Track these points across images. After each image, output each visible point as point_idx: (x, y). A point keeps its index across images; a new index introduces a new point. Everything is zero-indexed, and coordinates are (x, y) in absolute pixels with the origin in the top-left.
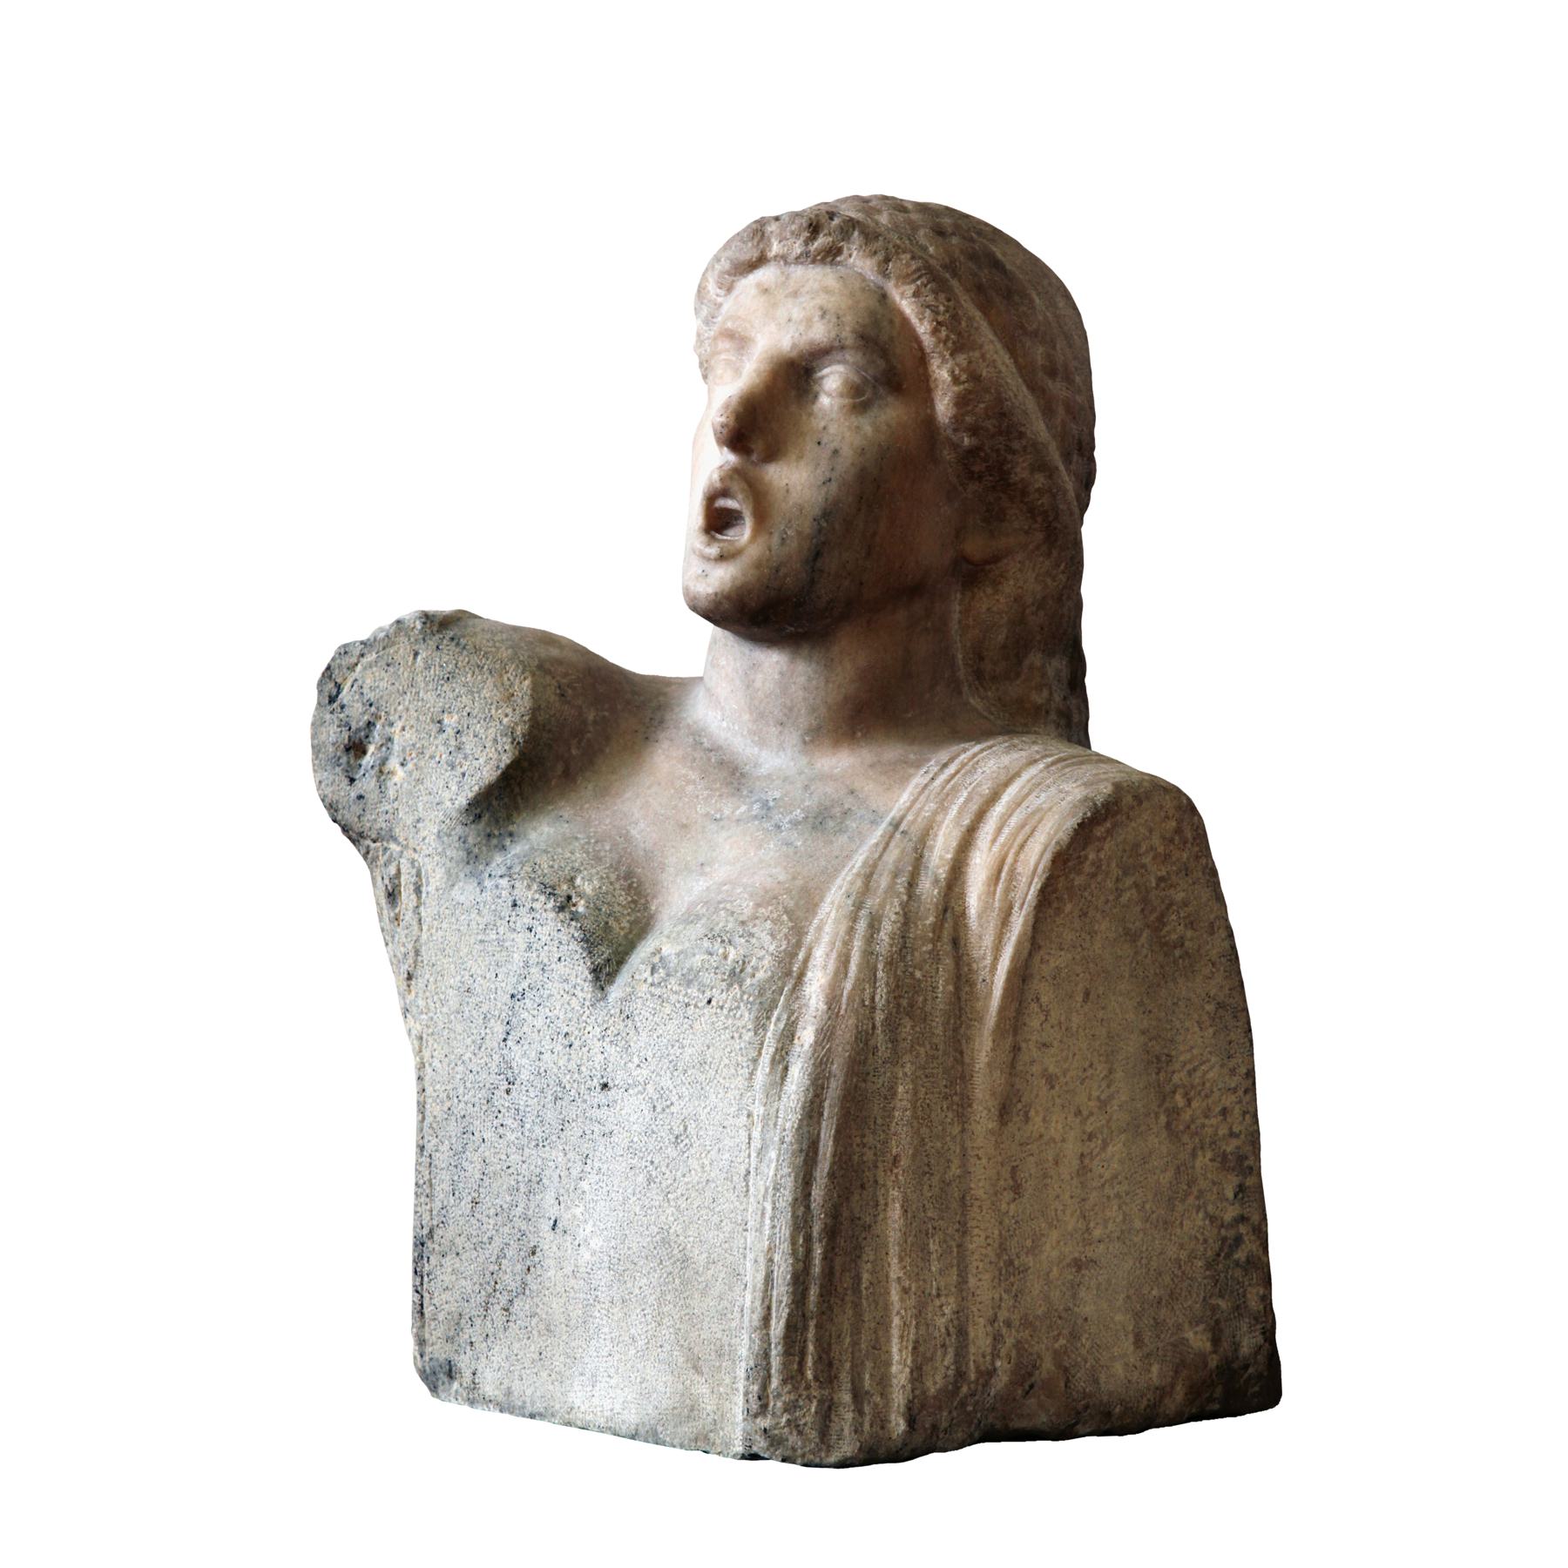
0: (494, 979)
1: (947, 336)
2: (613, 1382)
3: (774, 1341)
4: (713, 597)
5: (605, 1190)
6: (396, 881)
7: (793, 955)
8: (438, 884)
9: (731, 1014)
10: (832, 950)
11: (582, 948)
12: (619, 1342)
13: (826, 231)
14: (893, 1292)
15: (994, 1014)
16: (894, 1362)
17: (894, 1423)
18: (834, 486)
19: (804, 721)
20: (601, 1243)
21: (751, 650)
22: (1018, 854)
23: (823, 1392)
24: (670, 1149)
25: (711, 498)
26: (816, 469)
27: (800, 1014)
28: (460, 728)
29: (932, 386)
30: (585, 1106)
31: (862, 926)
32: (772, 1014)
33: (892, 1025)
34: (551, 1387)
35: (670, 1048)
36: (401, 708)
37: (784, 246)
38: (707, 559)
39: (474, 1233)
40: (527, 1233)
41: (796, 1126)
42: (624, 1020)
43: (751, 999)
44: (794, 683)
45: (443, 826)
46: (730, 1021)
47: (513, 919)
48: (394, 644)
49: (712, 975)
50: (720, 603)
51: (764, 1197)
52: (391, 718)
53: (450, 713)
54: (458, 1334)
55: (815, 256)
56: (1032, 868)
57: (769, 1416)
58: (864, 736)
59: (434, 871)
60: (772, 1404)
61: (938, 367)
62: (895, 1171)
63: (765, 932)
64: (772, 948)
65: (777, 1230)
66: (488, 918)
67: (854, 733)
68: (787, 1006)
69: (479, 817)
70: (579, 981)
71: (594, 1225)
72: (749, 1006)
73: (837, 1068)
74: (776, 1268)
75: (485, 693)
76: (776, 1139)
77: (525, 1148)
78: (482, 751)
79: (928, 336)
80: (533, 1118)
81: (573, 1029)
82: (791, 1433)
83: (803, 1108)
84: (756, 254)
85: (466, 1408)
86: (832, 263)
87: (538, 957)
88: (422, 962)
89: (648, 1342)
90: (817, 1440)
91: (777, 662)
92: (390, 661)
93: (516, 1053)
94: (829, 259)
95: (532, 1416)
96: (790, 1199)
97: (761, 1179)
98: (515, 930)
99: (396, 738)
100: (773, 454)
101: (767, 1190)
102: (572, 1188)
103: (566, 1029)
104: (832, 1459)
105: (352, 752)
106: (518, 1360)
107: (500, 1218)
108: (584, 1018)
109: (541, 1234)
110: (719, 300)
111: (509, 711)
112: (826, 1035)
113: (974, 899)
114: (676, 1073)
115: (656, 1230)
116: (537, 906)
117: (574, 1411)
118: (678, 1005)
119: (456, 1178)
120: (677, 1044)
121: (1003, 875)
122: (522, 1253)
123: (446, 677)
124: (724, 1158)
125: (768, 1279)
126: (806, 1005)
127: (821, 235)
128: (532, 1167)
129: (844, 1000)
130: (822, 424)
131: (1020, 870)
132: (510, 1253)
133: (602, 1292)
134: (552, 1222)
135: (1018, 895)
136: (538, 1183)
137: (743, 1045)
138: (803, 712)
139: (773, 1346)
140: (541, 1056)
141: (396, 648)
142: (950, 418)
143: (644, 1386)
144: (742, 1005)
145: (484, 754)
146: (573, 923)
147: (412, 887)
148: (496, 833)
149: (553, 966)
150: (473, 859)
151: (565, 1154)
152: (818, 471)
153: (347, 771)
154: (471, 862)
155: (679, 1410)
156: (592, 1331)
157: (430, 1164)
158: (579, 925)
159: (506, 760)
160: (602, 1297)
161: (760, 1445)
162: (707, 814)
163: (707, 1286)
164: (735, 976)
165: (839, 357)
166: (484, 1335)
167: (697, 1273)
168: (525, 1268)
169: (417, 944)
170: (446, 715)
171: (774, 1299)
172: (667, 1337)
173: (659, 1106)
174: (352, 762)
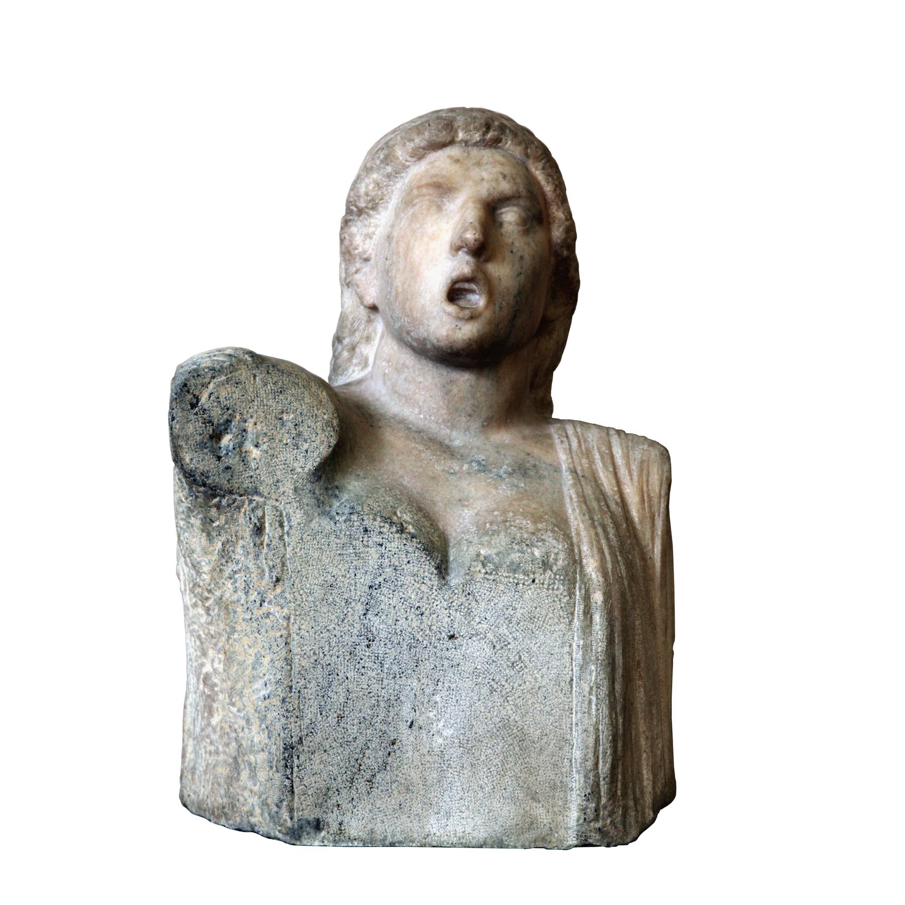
0: (353, 577)
1: (560, 193)
2: (464, 815)
3: (602, 776)
4: (468, 341)
6: (263, 520)
7: (573, 551)
8: (299, 520)
9: (550, 587)
10: (592, 546)
11: (425, 554)
12: (469, 790)
13: (493, 128)
14: (642, 739)
15: (659, 576)
16: (645, 779)
17: (647, 814)
18: (522, 277)
19: (485, 413)
20: (452, 732)
21: (448, 372)
22: (647, 486)
25: (455, 282)
26: (513, 267)
27: (589, 584)
29: (551, 221)
30: (435, 650)
31: (600, 530)
32: (576, 586)
34: (410, 825)
35: (505, 610)
36: (251, 411)
37: (468, 135)
38: (459, 319)
40: (388, 731)
41: (605, 649)
42: (466, 596)
43: (562, 578)
44: (479, 391)
45: (298, 484)
46: (551, 591)
47: (366, 539)
48: (237, 370)
49: (531, 565)
50: (472, 345)
51: (590, 694)
52: (245, 417)
53: (287, 413)
54: (326, 801)
55: (488, 142)
56: (658, 493)
57: (601, 821)
58: (510, 422)
59: (294, 513)
60: (602, 813)
61: (556, 210)
62: (639, 670)
63: (551, 538)
64: (560, 547)
65: (600, 711)
66: (344, 540)
67: (507, 420)
68: (582, 581)
69: (320, 477)
70: (426, 574)
71: (446, 722)
72: (561, 582)
73: (616, 613)
74: (601, 733)
75: (307, 400)
77: (384, 680)
78: (316, 436)
79: (551, 193)
80: (392, 661)
81: (424, 604)
82: (612, 828)
83: (607, 638)
84: (449, 139)
85: (523, 850)
86: (496, 148)
88: (287, 570)
89: (494, 788)
91: (468, 380)
92: (237, 381)
93: (375, 622)
94: (494, 145)
95: (392, 845)
96: (607, 692)
97: (585, 683)
98: (368, 546)
99: (250, 430)
101: (591, 688)
102: (426, 700)
103: (418, 605)
104: (629, 840)
105: (214, 439)
106: (380, 811)
107: (363, 725)
108: (433, 597)
109: (400, 732)
110: (407, 163)
111: (325, 411)
112: (607, 596)
113: (635, 514)
114: (511, 625)
115: (498, 720)
116: (385, 530)
117: (430, 837)
118: (509, 585)
119: (323, 703)
120: (511, 608)
121: (646, 498)
122: (383, 745)
123: (279, 390)
124: (552, 672)
125: (597, 740)
126: (590, 579)
127: (491, 130)
128: (391, 691)
129: (610, 574)
130: (510, 241)
131: (652, 495)
132: (372, 745)
133: (454, 762)
134: (409, 723)
136: (396, 700)
138: (484, 408)
139: (601, 779)
140: (396, 623)
141: (240, 372)
142: (562, 240)
143: (491, 814)
144: (556, 581)
145: (318, 438)
146: (414, 540)
147: (277, 524)
148: (330, 487)
149: (404, 566)
150: (321, 505)
151: (420, 681)
153: (213, 452)
154: (321, 505)
155: (521, 825)
156: (445, 786)
157: (299, 697)
158: (418, 541)
159: (333, 442)
161: (595, 837)
163: (541, 749)
164: (546, 565)
165: (516, 202)
167: (533, 742)
169: (284, 559)
170: (285, 414)
171: (601, 752)
172: (510, 783)
173: (499, 644)
174: (214, 446)
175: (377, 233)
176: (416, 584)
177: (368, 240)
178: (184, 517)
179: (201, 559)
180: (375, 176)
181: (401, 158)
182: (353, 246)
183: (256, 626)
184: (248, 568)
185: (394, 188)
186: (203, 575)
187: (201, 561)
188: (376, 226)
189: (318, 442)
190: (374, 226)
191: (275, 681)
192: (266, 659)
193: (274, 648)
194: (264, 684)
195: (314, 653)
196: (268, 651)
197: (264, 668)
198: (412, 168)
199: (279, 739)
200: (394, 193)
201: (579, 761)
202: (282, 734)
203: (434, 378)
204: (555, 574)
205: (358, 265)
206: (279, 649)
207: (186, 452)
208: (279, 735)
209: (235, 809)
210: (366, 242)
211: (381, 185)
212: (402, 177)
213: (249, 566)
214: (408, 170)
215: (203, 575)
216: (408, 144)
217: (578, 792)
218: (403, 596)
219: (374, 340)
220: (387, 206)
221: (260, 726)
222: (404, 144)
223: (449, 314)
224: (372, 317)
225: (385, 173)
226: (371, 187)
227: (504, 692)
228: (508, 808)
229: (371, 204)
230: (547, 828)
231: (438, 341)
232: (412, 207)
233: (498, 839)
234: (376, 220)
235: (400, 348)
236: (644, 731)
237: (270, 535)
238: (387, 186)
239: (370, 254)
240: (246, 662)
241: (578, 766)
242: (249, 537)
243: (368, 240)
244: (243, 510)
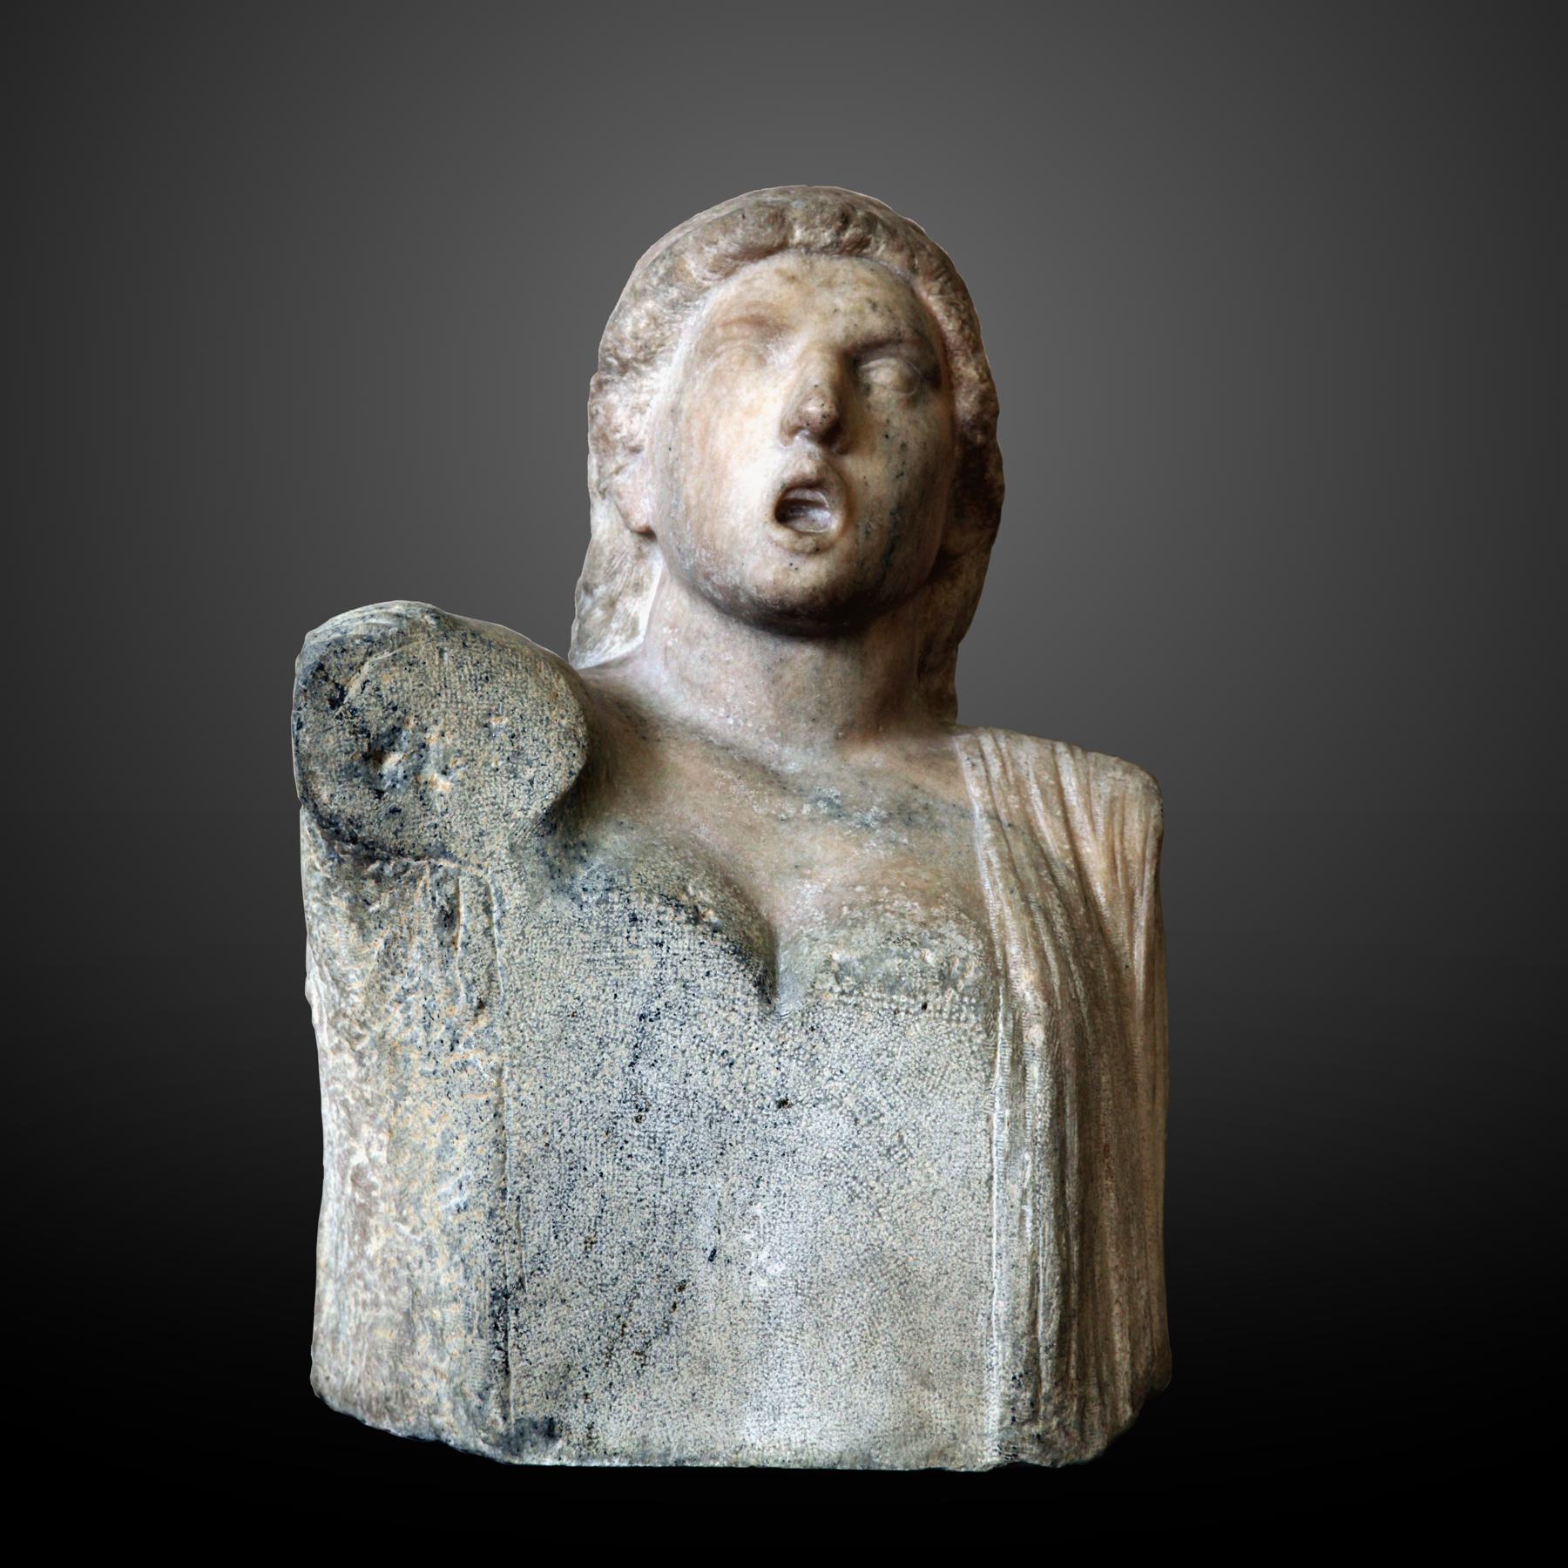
0: (612, 1000)
1: (970, 335)
2: (804, 1412)
3: (1043, 1344)
4: (810, 590)
6: (455, 902)
7: (992, 954)
8: (518, 902)
9: (954, 1017)
10: (1026, 946)
11: (737, 960)
12: (813, 1369)
13: (855, 222)
14: (1112, 1281)
15: (1142, 998)
16: (1117, 1350)
17: (1121, 1410)
18: (905, 480)
19: (840, 716)
20: (784, 1268)
21: (777, 645)
22: (1122, 842)
23: (446, 1405)
24: (879, 1162)
25: (788, 489)
26: (889, 462)
27: (1021, 1012)
28: (514, 731)
30: (754, 1127)
31: (1039, 919)
32: (998, 1015)
33: (1092, 1017)
34: (710, 1429)
35: (874, 1057)
36: (434, 711)
37: (811, 234)
38: (795, 552)
39: (589, 1276)
40: (672, 1267)
41: (1047, 1125)
42: (807, 1033)
43: (974, 1001)
44: (831, 678)
45: (516, 838)
46: (954, 1025)
47: (633, 934)
48: (410, 641)
49: (920, 979)
50: (817, 598)
51: (1023, 1202)
52: (424, 722)
53: (498, 715)
54: (565, 1388)
55: (846, 247)
56: (1141, 855)
57: (1041, 1422)
58: (884, 731)
59: (510, 889)
60: (1042, 1408)
61: (964, 365)
62: (1107, 1161)
63: (955, 932)
64: (971, 948)
65: (1040, 1232)
66: (596, 935)
67: (878, 727)
68: (1009, 1007)
69: (554, 827)
70: (739, 994)
71: (772, 1250)
72: (973, 1008)
73: (1068, 1062)
74: (1041, 1270)
77: (665, 1178)
78: (547, 756)
79: (955, 334)
82: (1060, 1435)
83: (1051, 1106)
84: (778, 240)
86: (859, 256)
88: (498, 987)
89: (856, 1365)
91: (811, 658)
92: (411, 660)
93: (650, 1078)
94: (857, 251)
96: (1052, 1199)
97: (1014, 1183)
98: (638, 946)
99: (432, 745)
100: (844, 451)
101: (1024, 1192)
102: (739, 1213)
103: (724, 1047)
105: (371, 761)
106: (658, 1406)
107: (628, 1256)
108: (749, 1034)
109: (693, 1267)
110: (706, 283)
111: (562, 712)
112: (1052, 1032)
113: (1100, 890)
114: (885, 1083)
115: (864, 1247)
116: (667, 918)
117: (745, 1451)
118: (883, 1013)
119: (559, 1218)
120: (885, 1053)
121: (1118, 862)
122: (663, 1290)
123: (484, 676)
125: (1034, 1283)
126: (1023, 1003)
127: (851, 226)
128: (678, 1197)
129: (1057, 994)
130: (884, 417)
131: (1130, 857)
132: (645, 1292)
133: (786, 1320)
134: (708, 1253)
135: (1135, 881)
136: (687, 1213)
137: (975, 1048)
138: (839, 707)
139: (1041, 1350)
140: (687, 1079)
141: (415, 644)
142: (973, 416)
143: (850, 1411)
144: (964, 1007)
145: (551, 758)
146: (718, 935)
147: (480, 908)
148: (571, 843)
149: (700, 981)
150: (557, 875)
151: (727, 1179)
153: (369, 783)
155: (902, 1430)
156: (770, 1362)
157: (518, 1207)
159: (577, 765)
160: (785, 1325)
162: (768, 815)
163: (937, 1298)
164: (946, 979)
165: (894, 350)
166: (607, 1384)
167: (924, 1286)
169: (491, 968)
170: (493, 718)
172: (883, 1356)
173: (865, 1116)
174: (371, 772)
175: (653, 403)
177: (638, 416)
178: (319, 896)
179: (348, 968)
180: (649, 305)
181: (694, 274)
182: (612, 427)
183: (444, 1084)
184: (430, 984)
185: (682, 326)
186: (352, 996)
187: (348, 972)
188: (652, 392)
189: (551, 766)
190: (648, 391)
191: (477, 1179)
192: (461, 1143)
193: (475, 1122)
194: (458, 1184)
195: (545, 1132)
196: (464, 1127)
197: (457, 1157)
198: (714, 290)
199: (483, 1281)
200: (683, 334)
201: (1003, 1318)
202: (488, 1272)
203: (751, 655)
204: (962, 995)
205: (620, 459)
206: (483, 1124)
207: (323, 784)
208: (484, 1273)
209: (407, 1402)
210: (634, 419)
211: (660, 321)
212: (696, 307)
213: (431, 981)
214: (706, 294)
215: (352, 996)
216: (706, 249)
217: (1002, 1372)
218: (699, 1033)
219: (647, 589)
220: (671, 357)
221: (451, 1258)
222: (701, 250)
223: (778, 544)
224: (645, 549)
225: (667, 300)
226: (642, 324)
229: (642, 353)
231: (759, 590)
232: (714, 359)
233: (863, 1454)
234: (652, 382)
235: (694, 603)
236: (1116, 1267)
237: (469, 927)
239: (641, 441)
240: (427, 1147)
241: (1002, 1326)
242: (431, 931)
243: (638, 416)
244: (421, 884)
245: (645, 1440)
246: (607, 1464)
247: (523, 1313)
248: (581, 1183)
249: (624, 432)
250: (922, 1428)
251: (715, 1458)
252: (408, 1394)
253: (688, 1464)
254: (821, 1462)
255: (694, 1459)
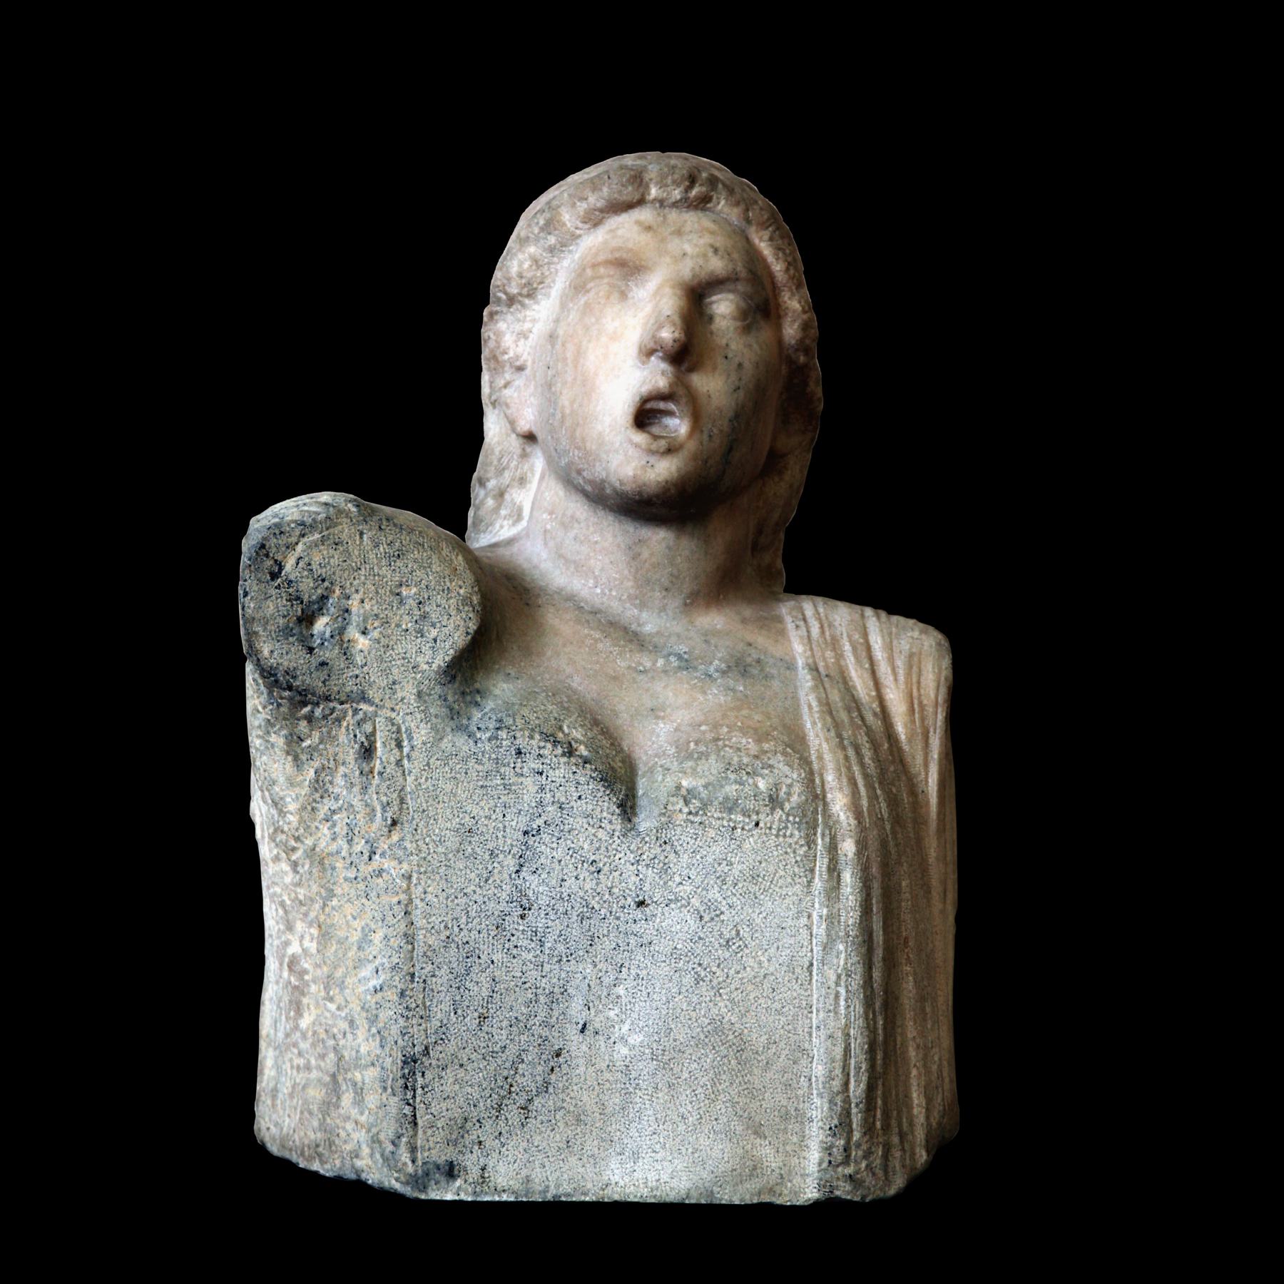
0: (501, 819)
1: (794, 274)
3: (854, 1101)
4: (664, 484)
5: (644, 993)
6: (373, 738)
7: (813, 781)
8: (424, 738)
9: (781, 833)
10: (841, 775)
11: (604, 786)
12: (665, 1121)
13: (700, 182)
14: (911, 1049)
15: (935, 817)
16: (915, 1105)
17: (918, 1155)
18: (741, 393)
19: (688, 587)
20: (642, 1038)
21: (636, 528)
22: (919, 689)
23: (366, 1151)
25: (645, 400)
26: (728, 379)
27: (836, 829)
29: (782, 313)
30: (617, 923)
31: (851, 752)
32: (817, 831)
34: (581, 1170)
35: (716, 866)
36: (355, 583)
37: (664, 192)
38: (651, 452)
39: (483, 1045)
40: (550, 1037)
41: (858, 921)
42: (661, 846)
43: (797, 819)
44: (680, 555)
45: (422, 686)
46: (781, 839)
47: (519, 765)
48: (336, 525)
49: (753, 802)
50: (669, 489)
51: (837, 984)
52: (347, 591)
53: (408, 586)
54: (463, 1137)
55: (692, 202)
56: (934, 700)
57: (852, 1164)
58: (724, 599)
59: (418, 728)
60: (854, 1153)
61: (790, 299)
62: (906, 951)
64: (795, 776)
65: (852, 1008)
66: (488, 766)
67: (719, 595)
68: (826, 824)
69: (454, 677)
70: (605, 814)
71: (632, 1024)
72: (796, 825)
73: (875, 870)
74: (853, 1040)
76: (842, 934)
77: (545, 964)
78: (448, 619)
79: (782, 273)
82: (868, 1175)
83: (861, 906)
84: (637, 197)
86: (703, 209)
87: (554, 797)
88: (408, 808)
89: (701, 1118)
90: (883, 1178)
91: (664, 539)
92: (337, 540)
93: (532, 883)
94: (701, 205)
96: (861, 982)
98: (522, 775)
99: (354, 610)
100: (691, 370)
101: (839, 976)
102: (605, 993)
103: (593, 858)
105: (304, 623)
106: (539, 1151)
107: (514, 1028)
108: (614, 846)
109: (567, 1038)
110: (578, 232)
111: (460, 583)
112: (862, 845)
113: (900, 729)
114: (725, 887)
115: (707, 1021)
116: (546, 752)
117: (610, 1188)
118: (723, 830)
119: (458, 998)
120: (725, 862)
121: (916, 706)
122: (543, 1056)
123: (396, 554)
124: (783, 954)
125: (847, 1051)
126: (838, 822)
127: (697, 185)
128: (555, 980)
129: (866, 814)
130: (724, 342)
131: (925, 702)
132: (528, 1058)
133: (644, 1081)
134: (580, 1026)
135: (930, 721)
136: (562, 994)
137: (799, 859)
138: (687, 579)
139: (853, 1105)
140: (563, 884)
141: (340, 527)
142: (797, 341)
143: (696, 1155)
144: (789, 825)
145: (451, 621)
146: (588, 766)
147: (393, 743)
148: (468, 690)
149: (573, 803)
150: (456, 716)
151: (595, 966)
152: (730, 380)
153: (302, 641)
155: (739, 1171)
156: (631, 1115)
157: (424, 989)
158: (593, 767)
159: (473, 627)
162: (629, 667)
163: (767, 1063)
164: (774, 801)
165: (732, 287)
166: (497, 1134)
167: (757, 1053)
168: (548, 1069)
169: (402, 793)
170: (404, 588)
172: (723, 1111)
173: (708, 914)
174: (304, 632)
175: (534, 330)
176: (590, 829)
177: (522, 341)
178: (261, 733)
179: (285, 793)
180: (532, 249)
181: (569, 225)
182: (501, 350)
183: (364, 887)
185: (559, 267)
186: (288, 815)
187: (285, 796)
188: (534, 321)
190: (530, 321)
192: (377, 936)
193: (389, 919)
194: (375, 970)
195: (446, 927)
196: (380, 923)
197: (374, 948)
198: (585, 238)
199: (395, 1049)
200: (559, 274)
201: (821, 1079)
202: (400, 1041)
203: (615, 536)
204: (788, 815)
205: (508, 376)
206: (395, 920)
207: (264, 642)
208: (396, 1042)
209: (333, 1148)
210: (519, 343)
211: (540, 263)
212: (570, 252)
213: (353, 803)
214: (578, 241)
215: (288, 815)
216: (578, 204)
217: (820, 1124)
219: (530, 482)
220: (550, 292)
221: (369, 1030)
222: (574, 205)
223: (637, 446)
224: (528, 449)
225: (546, 246)
226: (526, 266)
227: (715, 982)
228: (720, 1147)
229: (526, 289)
230: (776, 1174)
231: (622, 483)
232: (585, 294)
233: (707, 1191)
234: (534, 312)
235: (568, 493)
237: (384, 759)
238: (549, 263)
239: (525, 361)
240: (350, 939)
241: (821, 1086)
242: (353, 762)
244: (345, 724)
245: (528, 1180)
246: (497, 1199)
247: (429, 1075)
248: (476, 969)
249: (511, 354)
250: (755, 1170)
251: (585, 1194)
252: (334, 1142)
253: (563, 1199)
254: (672, 1197)
255: (568, 1195)
